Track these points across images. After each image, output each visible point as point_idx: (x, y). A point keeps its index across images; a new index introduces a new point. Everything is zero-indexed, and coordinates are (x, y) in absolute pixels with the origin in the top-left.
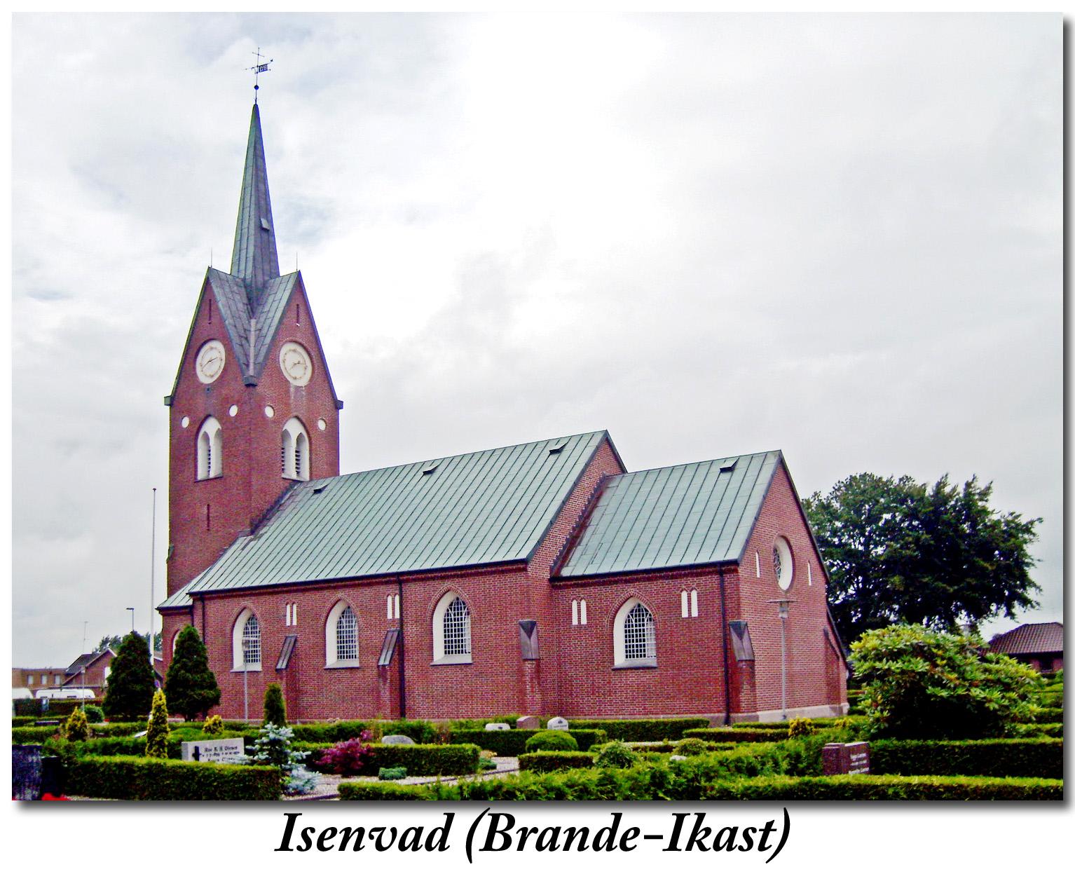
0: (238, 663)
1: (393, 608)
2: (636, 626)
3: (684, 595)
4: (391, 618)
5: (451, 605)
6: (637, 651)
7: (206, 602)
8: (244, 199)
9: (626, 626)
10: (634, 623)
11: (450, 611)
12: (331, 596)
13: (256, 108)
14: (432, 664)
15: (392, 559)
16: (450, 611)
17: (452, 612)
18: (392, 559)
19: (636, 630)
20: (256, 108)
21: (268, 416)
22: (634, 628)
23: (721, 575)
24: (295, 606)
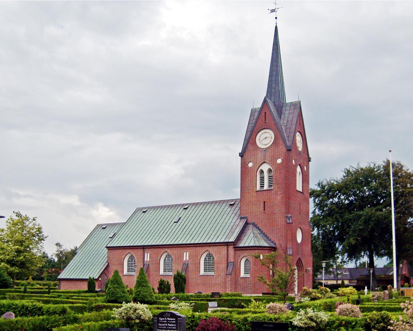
0: (242, 274)
1: (147, 258)
2: (208, 260)
3: (185, 253)
4: (185, 259)
5: (130, 257)
6: (212, 264)
7: (145, 249)
8: (272, 64)
9: (204, 261)
10: (207, 260)
11: (207, 257)
12: (163, 250)
13: (276, 27)
14: (199, 275)
15: (208, 237)
16: (207, 257)
17: (166, 259)
18: (208, 237)
19: (208, 262)
20: (276, 27)
21: (352, 267)
22: (208, 261)
23: (144, 249)
24: (149, 254)
